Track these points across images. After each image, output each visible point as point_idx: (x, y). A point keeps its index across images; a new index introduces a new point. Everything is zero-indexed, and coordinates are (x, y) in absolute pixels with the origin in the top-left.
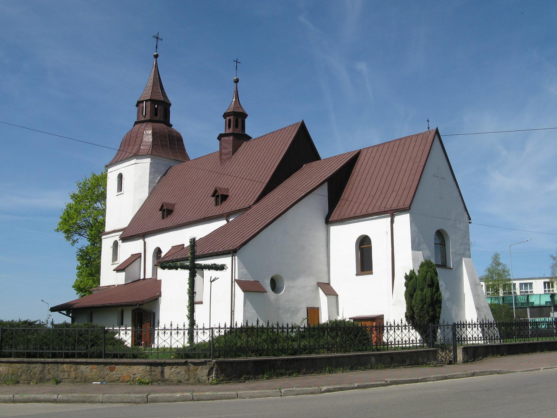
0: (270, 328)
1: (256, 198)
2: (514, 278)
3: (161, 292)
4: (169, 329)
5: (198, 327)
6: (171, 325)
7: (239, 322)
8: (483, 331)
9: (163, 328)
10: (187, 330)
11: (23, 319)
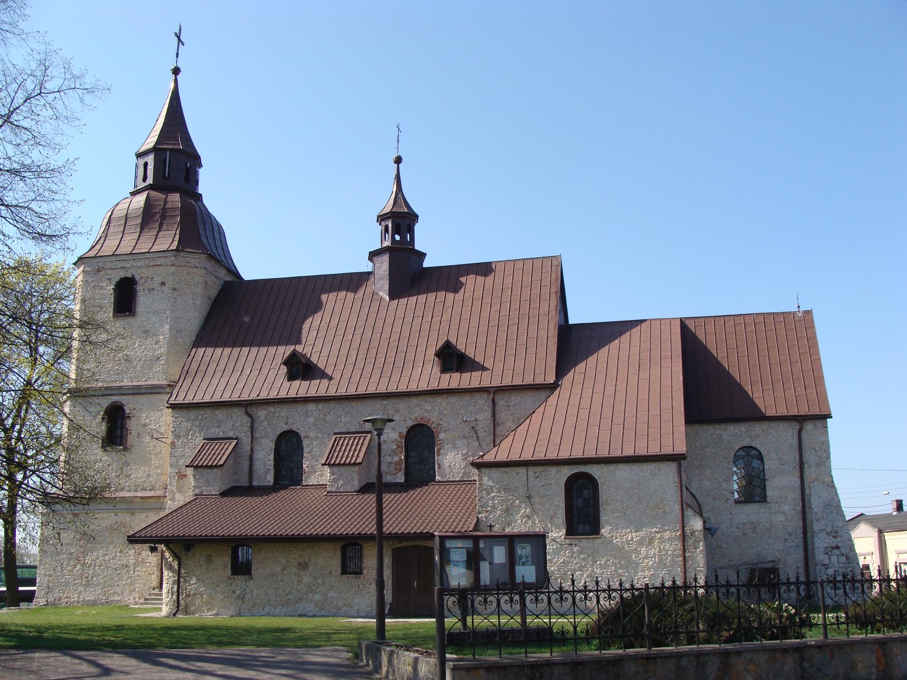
10: (744, 585)
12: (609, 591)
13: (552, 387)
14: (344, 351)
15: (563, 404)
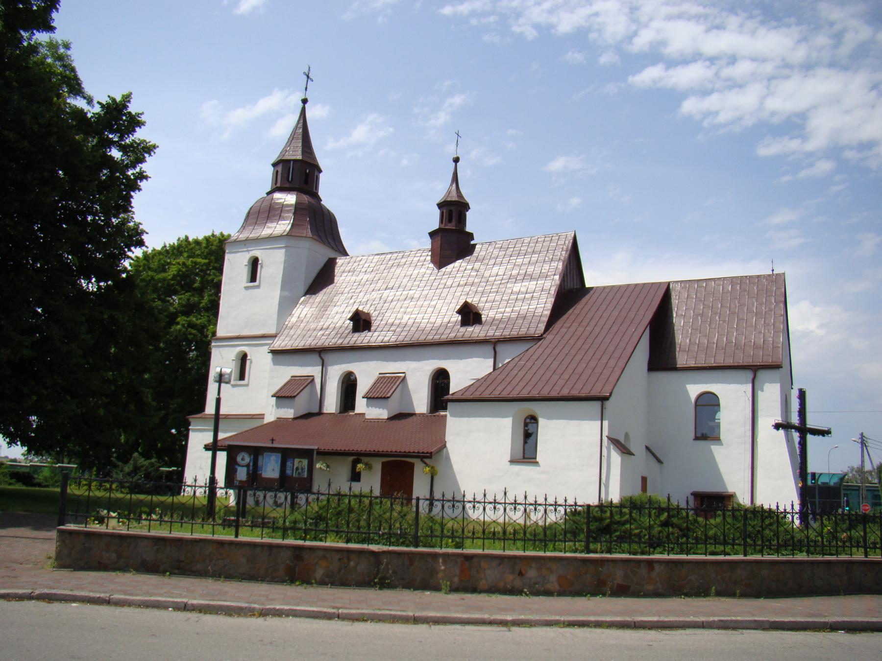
0: (782, 513)
1: (224, 539)
2: (522, 455)
3: (446, 442)
4: (501, 502)
5: (568, 501)
6: (526, 497)
7: (615, 495)
8: (822, 526)
9: (513, 502)
10: (692, 509)
11: (816, 436)
12: (556, 505)
13: (540, 338)
14: (622, 345)
15: (540, 351)
